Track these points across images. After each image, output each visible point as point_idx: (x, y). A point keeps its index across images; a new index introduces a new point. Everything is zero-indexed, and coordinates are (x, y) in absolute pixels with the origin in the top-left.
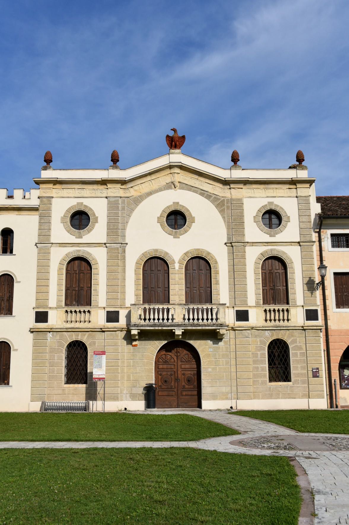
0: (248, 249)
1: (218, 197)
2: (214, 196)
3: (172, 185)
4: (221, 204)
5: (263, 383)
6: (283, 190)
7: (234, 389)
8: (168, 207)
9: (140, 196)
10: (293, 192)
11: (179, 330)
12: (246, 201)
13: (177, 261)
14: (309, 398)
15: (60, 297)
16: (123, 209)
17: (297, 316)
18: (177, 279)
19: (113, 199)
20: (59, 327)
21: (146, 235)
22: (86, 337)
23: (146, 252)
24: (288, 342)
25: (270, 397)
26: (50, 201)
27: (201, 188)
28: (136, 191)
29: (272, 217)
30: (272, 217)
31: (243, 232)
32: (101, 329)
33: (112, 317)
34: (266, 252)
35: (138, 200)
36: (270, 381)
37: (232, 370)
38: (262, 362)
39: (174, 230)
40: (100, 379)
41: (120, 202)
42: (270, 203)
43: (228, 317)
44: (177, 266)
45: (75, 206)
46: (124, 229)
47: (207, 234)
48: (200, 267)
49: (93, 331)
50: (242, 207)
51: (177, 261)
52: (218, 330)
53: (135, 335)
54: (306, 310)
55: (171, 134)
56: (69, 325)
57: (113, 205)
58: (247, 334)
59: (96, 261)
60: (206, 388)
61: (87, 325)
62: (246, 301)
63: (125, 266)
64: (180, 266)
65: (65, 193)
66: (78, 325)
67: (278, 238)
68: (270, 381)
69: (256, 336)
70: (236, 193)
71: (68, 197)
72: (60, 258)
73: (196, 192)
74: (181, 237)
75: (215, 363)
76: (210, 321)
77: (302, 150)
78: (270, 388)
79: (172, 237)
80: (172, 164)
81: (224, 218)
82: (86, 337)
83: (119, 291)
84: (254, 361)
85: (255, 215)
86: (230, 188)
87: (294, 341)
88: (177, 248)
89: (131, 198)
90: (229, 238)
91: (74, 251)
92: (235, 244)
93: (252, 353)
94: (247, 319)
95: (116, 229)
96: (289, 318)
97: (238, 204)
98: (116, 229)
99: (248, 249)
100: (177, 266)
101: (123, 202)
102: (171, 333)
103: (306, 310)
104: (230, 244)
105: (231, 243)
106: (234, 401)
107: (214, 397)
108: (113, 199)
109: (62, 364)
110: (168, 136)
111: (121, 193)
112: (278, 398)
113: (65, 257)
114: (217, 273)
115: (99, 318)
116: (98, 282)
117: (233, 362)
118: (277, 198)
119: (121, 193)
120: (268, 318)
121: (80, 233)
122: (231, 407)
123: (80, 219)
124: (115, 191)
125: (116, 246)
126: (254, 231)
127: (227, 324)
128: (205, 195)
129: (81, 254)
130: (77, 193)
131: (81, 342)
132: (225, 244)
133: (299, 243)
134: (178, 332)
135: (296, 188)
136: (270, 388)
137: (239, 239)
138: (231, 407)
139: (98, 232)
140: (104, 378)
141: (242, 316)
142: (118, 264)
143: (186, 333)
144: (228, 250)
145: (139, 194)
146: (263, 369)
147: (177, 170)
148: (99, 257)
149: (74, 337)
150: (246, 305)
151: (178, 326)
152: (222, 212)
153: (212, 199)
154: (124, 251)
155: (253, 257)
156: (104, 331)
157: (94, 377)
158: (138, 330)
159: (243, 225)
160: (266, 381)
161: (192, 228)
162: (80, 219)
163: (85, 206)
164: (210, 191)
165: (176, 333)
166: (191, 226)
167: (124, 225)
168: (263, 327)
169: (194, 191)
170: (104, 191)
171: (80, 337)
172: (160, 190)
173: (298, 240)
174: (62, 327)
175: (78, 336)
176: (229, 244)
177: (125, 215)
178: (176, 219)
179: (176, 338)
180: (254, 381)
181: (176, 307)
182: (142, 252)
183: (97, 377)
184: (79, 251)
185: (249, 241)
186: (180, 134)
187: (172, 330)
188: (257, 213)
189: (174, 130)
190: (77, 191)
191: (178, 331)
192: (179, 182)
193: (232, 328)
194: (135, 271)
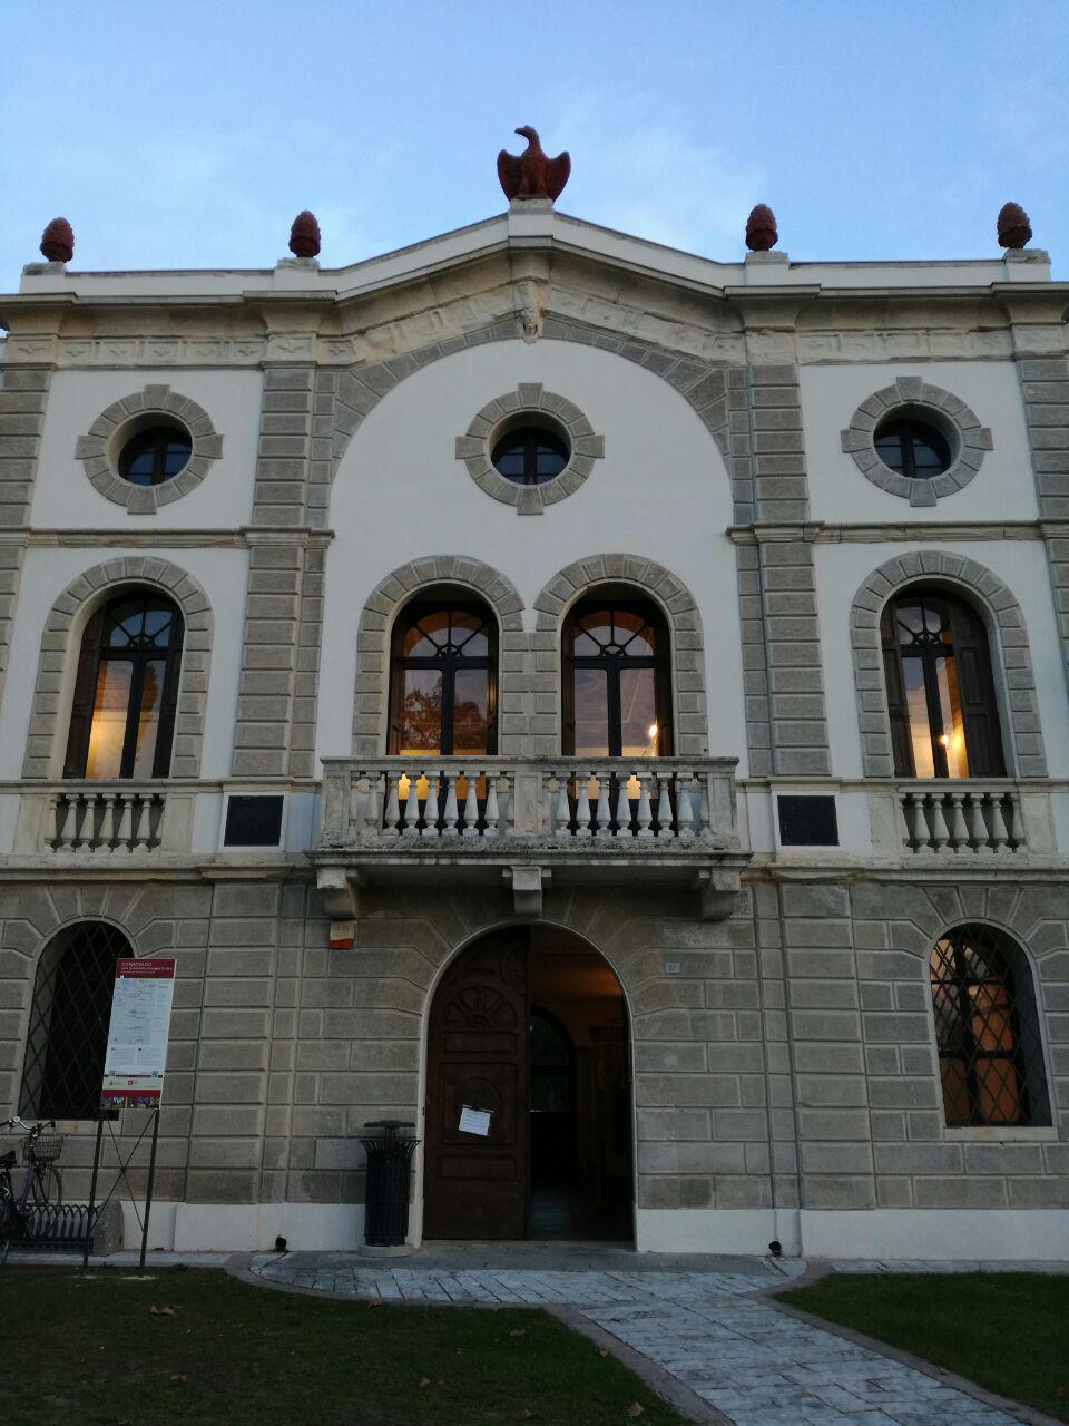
0: (826, 558)
1: (696, 363)
2: (679, 361)
3: (510, 326)
4: (710, 392)
5: (921, 1129)
6: (956, 339)
7: (783, 1152)
8: (500, 402)
9: (392, 364)
10: (999, 344)
11: (531, 870)
12: (805, 376)
13: (529, 597)
14: (801, 1206)
15: (37, 741)
16: (324, 407)
17: (1051, 825)
18: (529, 671)
19: (285, 373)
20: (23, 864)
21: (405, 497)
22: (132, 906)
23: (405, 568)
24: (1025, 939)
25: (957, 1196)
26: (42, 380)
27: (630, 330)
28: (375, 345)
29: (916, 438)
30: (916, 438)
31: (801, 488)
32: (198, 870)
33: (253, 820)
34: (894, 563)
35: (383, 378)
36: (951, 1123)
37: (773, 1064)
38: (915, 1030)
39: (521, 487)
40: (134, 1097)
41: (311, 383)
42: (906, 383)
43: (754, 825)
44: (529, 620)
45: (136, 397)
46: (324, 479)
47: (652, 493)
48: (622, 613)
49: (163, 882)
50: (794, 395)
51: (529, 597)
52: (703, 875)
53: (332, 892)
54: (780, 798)
55: (518, 147)
56: (64, 858)
57: (283, 395)
58: (830, 900)
59: (203, 598)
60: (657, 1147)
61: (141, 857)
62: (823, 759)
63: (317, 620)
64: (541, 619)
65: (104, 353)
66: (102, 857)
67: (949, 509)
68: (951, 1123)
69: (875, 914)
70: (764, 349)
71: (113, 368)
72: (60, 587)
73: (610, 348)
74: (547, 510)
75: (695, 1030)
76: (666, 833)
77: (1014, 200)
78: (953, 1153)
79: (514, 510)
80: (514, 243)
81: (720, 438)
82: (132, 906)
83: (289, 717)
84: (870, 1024)
85: (846, 427)
86: (743, 332)
87: (1051, 938)
88: (530, 554)
89: (356, 370)
90: (740, 513)
91: (118, 564)
92: (772, 537)
93: (861, 989)
94: (828, 835)
95: (292, 476)
96: (1019, 831)
97: (783, 384)
98: (292, 476)
99: (826, 558)
100: (529, 620)
101: (325, 386)
102: (495, 889)
103: (780, 798)
104: (745, 535)
105: (751, 529)
106: (785, 1215)
107: (693, 1192)
108: (285, 373)
109: (14, 1028)
110: (505, 161)
111: (320, 353)
112: (994, 1203)
113: (80, 585)
114: (695, 647)
115: (196, 829)
116: (203, 681)
117: (774, 1028)
118: (933, 366)
119: (320, 353)
120: (923, 831)
121: (148, 493)
122: (775, 1247)
123: (154, 446)
124: (298, 343)
125: (288, 549)
126: (841, 485)
127: (744, 849)
128: (646, 357)
129: (141, 574)
130: (149, 353)
131: (110, 929)
132: (729, 532)
133: (1037, 525)
134: (527, 881)
135: (1009, 328)
136: (953, 1153)
137: (784, 513)
138: (775, 1247)
139: (220, 492)
140: (156, 1094)
141: (809, 820)
142: (291, 609)
143: (561, 886)
144: (741, 558)
145: (389, 357)
146: (916, 1063)
147: (534, 270)
148: (219, 586)
149: (81, 909)
150: (822, 773)
151: (526, 853)
152: (711, 417)
153: (671, 369)
154: (318, 564)
155: (842, 582)
156: (211, 883)
157: (106, 1085)
158: (348, 867)
159: (800, 463)
160: (933, 1118)
161: (591, 477)
162: (154, 446)
163: (178, 398)
164: (665, 343)
165: (516, 886)
166: (589, 470)
167: (324, 469)
168: (903, 870)
169: (601, 345)
170: (253, 347)
171: (105, 909)
172: (471, 340)
173: (1031, 514)
174: (34, 863)
175: (98, 901)
176: (745, 535)
177: (327, 431)
178: (532, 446)
179: (520, 906)
180: (874, 1121)
181: (521, 770)
182: (393, 568)
183: (123, 1085)
184: (136, 561)
185: (828, 521)
186: (551, 151)
187: (502, 867)
188: (856, 417)
189: (528, 133)
190: (148, 348)
191: (526, 876)
192: (545, 313)
193: (766, 870)
194: (361, 638)
